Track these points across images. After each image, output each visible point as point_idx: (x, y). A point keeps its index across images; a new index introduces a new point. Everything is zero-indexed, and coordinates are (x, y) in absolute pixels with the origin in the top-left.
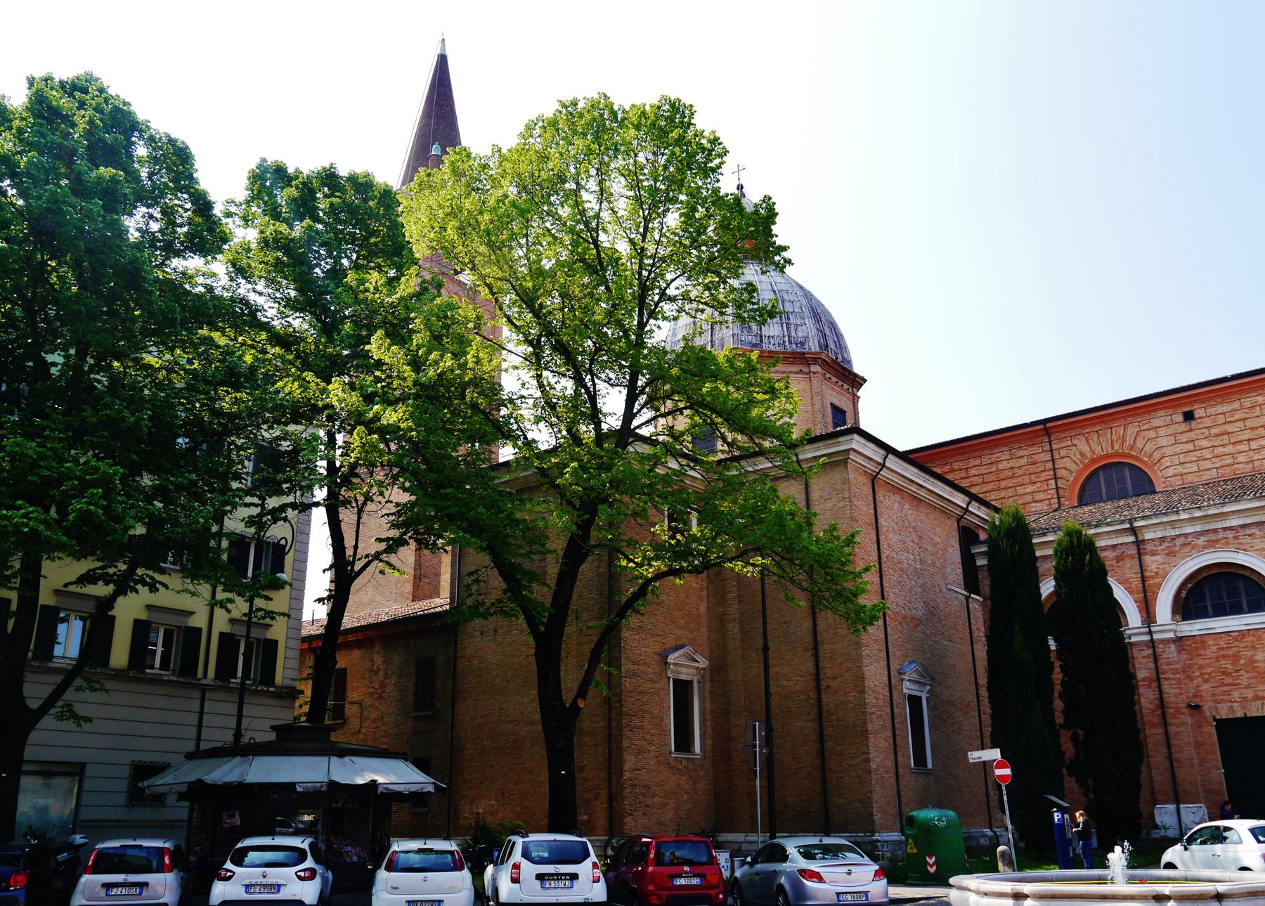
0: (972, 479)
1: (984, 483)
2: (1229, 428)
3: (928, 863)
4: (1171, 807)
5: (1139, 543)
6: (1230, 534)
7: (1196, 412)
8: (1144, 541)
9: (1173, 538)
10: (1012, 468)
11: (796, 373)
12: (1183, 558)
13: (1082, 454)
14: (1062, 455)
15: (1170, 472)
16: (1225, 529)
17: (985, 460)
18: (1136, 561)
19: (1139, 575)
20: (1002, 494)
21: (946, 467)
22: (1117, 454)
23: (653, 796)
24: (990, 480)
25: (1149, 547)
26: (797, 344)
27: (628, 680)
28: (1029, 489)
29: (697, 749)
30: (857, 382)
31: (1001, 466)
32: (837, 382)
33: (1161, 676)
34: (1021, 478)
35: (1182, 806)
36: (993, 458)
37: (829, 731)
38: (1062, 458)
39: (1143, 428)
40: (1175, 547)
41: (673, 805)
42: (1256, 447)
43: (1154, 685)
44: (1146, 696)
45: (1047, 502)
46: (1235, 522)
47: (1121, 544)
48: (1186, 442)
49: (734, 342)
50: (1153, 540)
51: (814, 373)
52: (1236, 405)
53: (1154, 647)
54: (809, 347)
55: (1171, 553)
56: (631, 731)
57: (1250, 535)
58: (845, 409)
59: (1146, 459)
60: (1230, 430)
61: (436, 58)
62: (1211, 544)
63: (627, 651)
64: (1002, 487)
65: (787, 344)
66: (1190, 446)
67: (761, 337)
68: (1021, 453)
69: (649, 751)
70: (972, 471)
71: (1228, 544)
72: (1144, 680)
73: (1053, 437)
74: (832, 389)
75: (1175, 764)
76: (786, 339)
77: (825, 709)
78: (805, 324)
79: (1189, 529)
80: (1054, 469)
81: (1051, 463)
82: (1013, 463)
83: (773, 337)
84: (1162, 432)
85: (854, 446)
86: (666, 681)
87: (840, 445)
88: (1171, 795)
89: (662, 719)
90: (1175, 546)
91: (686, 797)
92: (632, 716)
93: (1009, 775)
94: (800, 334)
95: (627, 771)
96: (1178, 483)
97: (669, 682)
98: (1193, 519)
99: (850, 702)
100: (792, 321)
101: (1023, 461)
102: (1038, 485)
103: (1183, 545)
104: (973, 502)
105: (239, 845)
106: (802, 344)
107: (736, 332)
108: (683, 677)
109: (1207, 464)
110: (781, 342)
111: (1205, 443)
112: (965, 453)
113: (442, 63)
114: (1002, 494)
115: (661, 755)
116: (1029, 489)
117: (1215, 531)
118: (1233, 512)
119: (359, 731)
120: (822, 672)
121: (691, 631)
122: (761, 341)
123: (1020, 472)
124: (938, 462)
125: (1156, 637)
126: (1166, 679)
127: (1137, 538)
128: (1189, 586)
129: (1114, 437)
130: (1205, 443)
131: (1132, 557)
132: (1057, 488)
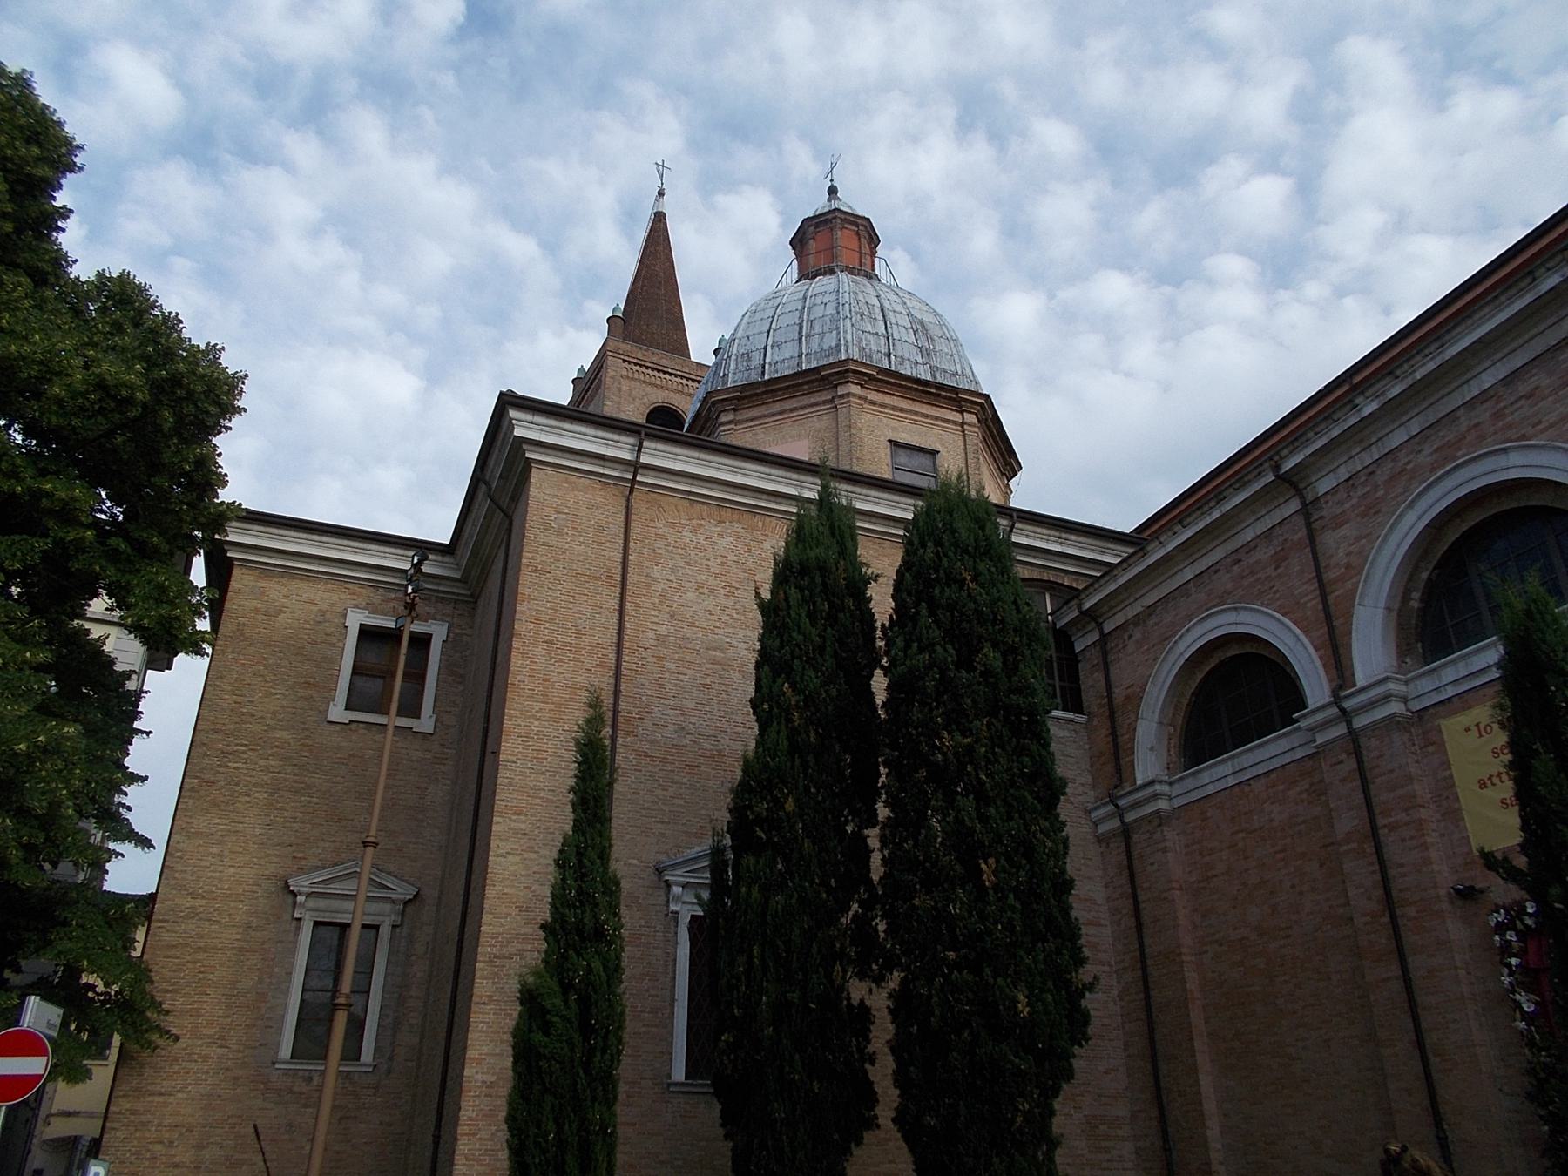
5: (1306, 511)
6: (1483, 413)
16: (1470, 404)
25: (1329, 510)
33: (1381, 821)
43: (1370, 848)
53: (1357, 752)
57: (1528, 397)
71: (1482, 438)
75: (1433, 1060)
78: (838, 328)
90: (1376, 488)
117: (1451, 416)
125: (1360, 722)
126: (1392, 828)
127: (1303, 498)
128: (1425, 575)
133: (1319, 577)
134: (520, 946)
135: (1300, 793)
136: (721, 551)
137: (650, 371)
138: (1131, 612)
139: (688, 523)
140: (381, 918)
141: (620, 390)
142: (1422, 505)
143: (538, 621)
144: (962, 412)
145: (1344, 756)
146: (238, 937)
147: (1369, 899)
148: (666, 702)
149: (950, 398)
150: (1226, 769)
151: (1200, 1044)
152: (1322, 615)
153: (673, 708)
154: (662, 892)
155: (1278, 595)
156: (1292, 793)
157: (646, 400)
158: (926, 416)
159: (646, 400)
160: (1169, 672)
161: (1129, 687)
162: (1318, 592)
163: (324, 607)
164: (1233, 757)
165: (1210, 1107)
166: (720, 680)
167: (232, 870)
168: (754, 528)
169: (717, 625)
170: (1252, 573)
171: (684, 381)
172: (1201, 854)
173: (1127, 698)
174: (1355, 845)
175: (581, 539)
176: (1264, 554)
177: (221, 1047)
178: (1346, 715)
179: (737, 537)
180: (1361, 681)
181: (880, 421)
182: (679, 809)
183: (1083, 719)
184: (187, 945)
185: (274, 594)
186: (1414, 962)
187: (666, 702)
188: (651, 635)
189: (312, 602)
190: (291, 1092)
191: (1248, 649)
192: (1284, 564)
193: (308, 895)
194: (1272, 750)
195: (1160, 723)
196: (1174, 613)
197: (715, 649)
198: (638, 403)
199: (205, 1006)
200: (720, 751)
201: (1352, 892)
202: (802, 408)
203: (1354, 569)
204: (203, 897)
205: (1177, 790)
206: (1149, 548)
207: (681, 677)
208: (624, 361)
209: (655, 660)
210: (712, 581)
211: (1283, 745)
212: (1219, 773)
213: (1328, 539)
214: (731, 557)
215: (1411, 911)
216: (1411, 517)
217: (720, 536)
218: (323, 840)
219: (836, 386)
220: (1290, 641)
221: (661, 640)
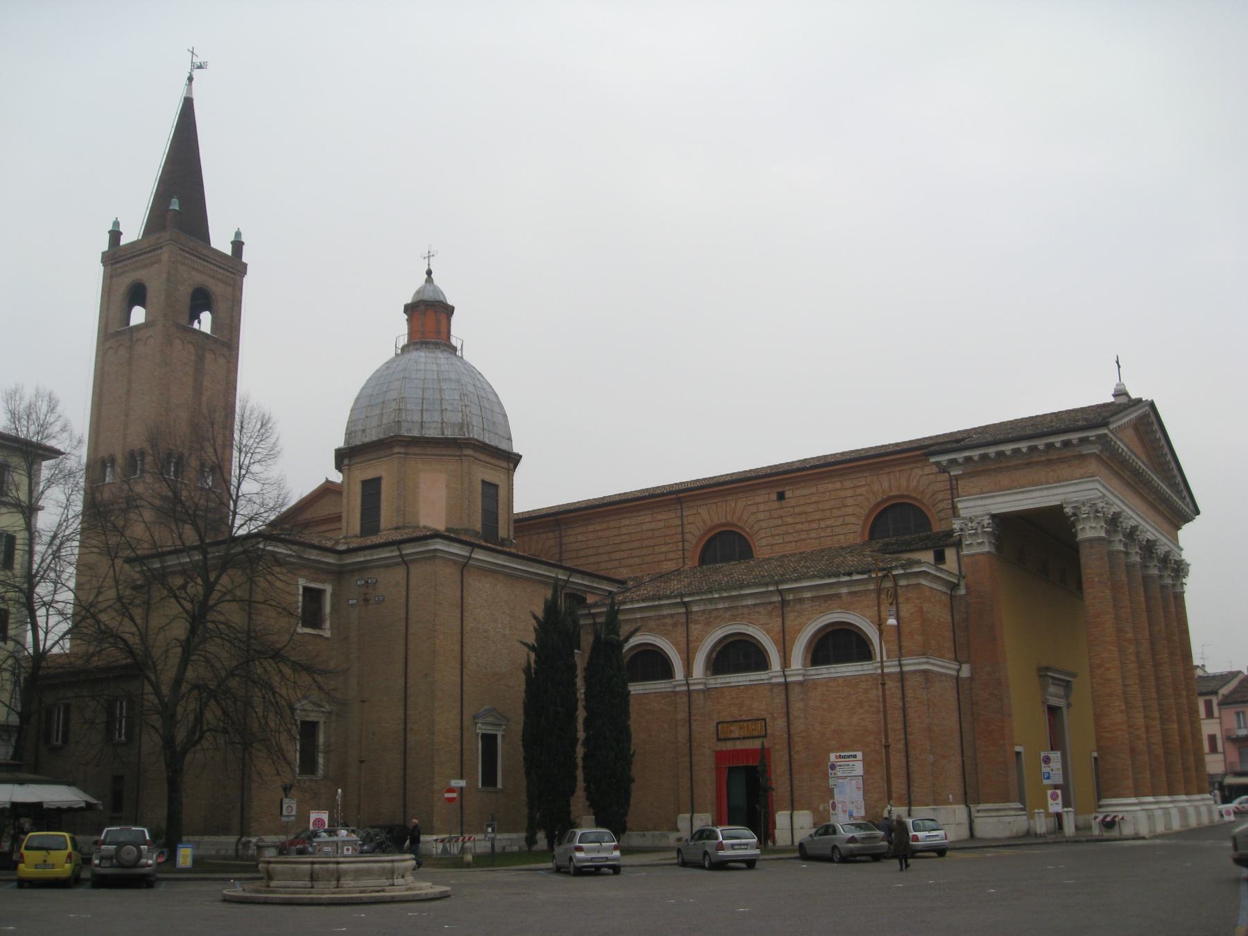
2: (808, 509)
4: (688, 816)
5: (688, 613)
6: (746, 611)
7: (786, 493)
9: (710, 612)
10: (653, 530)
12: (715, 628)
13: (704, 522)
14: (690, 521)
15: (764, 542)
16: (743, 606)
18: (685, 628)
19: (686, 639)
22: (727, 524)
28: (664, 549)
30: (514, 459)
31: (645, 527)
33: (692, 718)
35: (913, 808)
38: (690, 524)
39: (749, 503)
40: (711, 621)
42: (824, 526)
43: (688, 725)
45: (675, 561)
46: (750, 602)
47: (677, 614)
48: (778, 518)
50: (697, 612)
51: (465, 456)
52: (814, 490)
55: (708, 624)
59: (748, 530)
60: (808, 510)
61: (183, 99)
62: (734, 618)
66: (779, 522)
68: (660, 517)
70: (624, 530)
71: (743, 618)
73: (684, 506)
75: (694, 784)
79: (721, 606)
80: (683, 533)
81: (680, 528)
84: (762, 507)
85: (438, 547)
88: (907, 802)
96: (768, 552)
98: (722, 599)
101: (661, 524)
102: (670, 546)
103: (716, 618)
109: (789, 538)
111: (790, 520)
116: (664, 549)
117: (737, 607)
118: (748, 594)
125: (692, 688)
126: (695, 720)
127: (687, 610)
128: (718, 649)
129: (728, 508)
130: (790, 520)
132: (684, 550)
133: (687, 637)
142: (724, 630)
144: (508, 462)
145: (684, 696)
150: (641, 687)
170: (664, 626)
176: (669, 621)
178: (688, 684)
180: (694, 677)
183: (581, 652)
186: (694, 758)
202: (444, 455)
203: (700, 640)
208: (180, 249)
213: (692, 627)
215: (696, 744)
216: (719, 632)
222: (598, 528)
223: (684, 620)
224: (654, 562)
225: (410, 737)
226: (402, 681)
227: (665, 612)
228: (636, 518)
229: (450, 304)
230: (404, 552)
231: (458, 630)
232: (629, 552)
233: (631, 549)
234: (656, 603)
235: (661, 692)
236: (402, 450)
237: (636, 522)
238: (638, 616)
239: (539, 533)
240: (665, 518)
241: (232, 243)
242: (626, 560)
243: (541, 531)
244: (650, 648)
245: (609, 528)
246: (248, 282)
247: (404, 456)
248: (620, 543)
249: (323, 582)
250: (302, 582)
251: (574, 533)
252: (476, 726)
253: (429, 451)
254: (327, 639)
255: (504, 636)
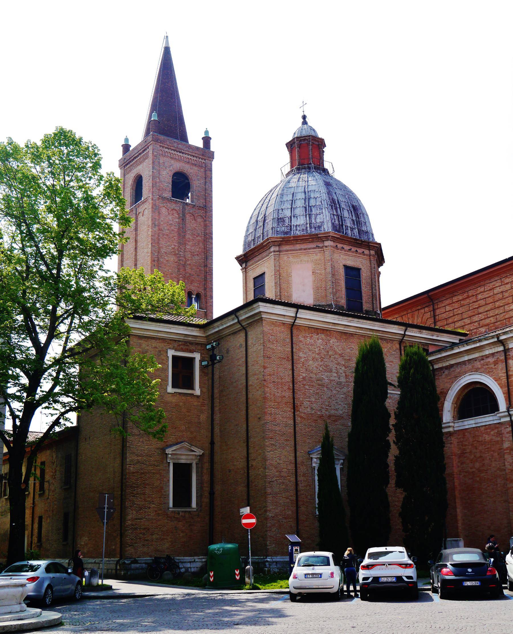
0: (479, 302)
1: (486, 304)
3: (236, 574)
8: (509, 349)
10: (502, 292)
11: (313, 248)
17: (487, 288)
20: (497, 312)
21: (465, 295)
23: (152, 535)
24: (489, 302)
26: (315, 228)
27: (132, 466)
29: (194, 504)
31: (496, 291)
32: (350, 250)
34: (507, 299)
36: (491, 285)
37: (252, 493)
41: (170, 540)
44: (508, 460)
47: (497, 352)
49: (272, 233)
51: (326, 247)
54: (324, 228)
56: (134, 496)
58: (360, 266)
61: (163, 49)
63: (131, 449)
64: (496, 306)
65: (308, 229)
67: (291, 226)
69: (149, 508)
70: (480, 297)
72: (507, 449)
74: (346, 255)
76: (308, 225)
77: (250, 479)
78: (322, 213)
82: (503, 288)
83: (299, 226)
85: (261, 309)
86: (167, 465)
87: (255, 310)
89: (162, 488)
91: (182, 534)
92: (135, 487)
93: (243, 519)
94: (318, 220)
95: (129, 520)
97: (169, 465)
99: (260, 475)
100: (314, 212)
104: (408, 329)
105: (257, 585)
106: (319, 227)
107: (274, 226)
108: (183, 460)
110: (305, 228)
112: (476, 283)
113: (167, 52)
114: (497, 312)
115: (161, 510)
119: (48, 498)
120: (250, 455)
121: (192, 433)
122: (291, 229)
123: (506, 294)
124: (460, 292)
127: (504, 347)
131: (501, 361)
133: (507, 372)
134: (276, 478)
135: (494, 433)
136: (318, 345)
137: (173, 152)
138: (444, 365)
139: (308, 335)
140: (192, 461)
141: (159, 163)
143: (270, 375)
144: (369, 250)
145: (508, 426)
146: (152, 469)
147: (511, 466)
148: (307, 399)
149: (366, 245)
150: (472, 422)
151: (458, 501)
152: (506, 384)
153: (309, 401)
154: (310, 460)
155: (494, 374)
156: (492, 433)
157: (171, 168)
158: (140, 154)
159: (171, 168)
160: (457, 388)
161: (442, 389)
162: (506, 377)
163: (160, 349)
164: (475, 419)
165: (459, 518)
166: (321, 391)
167: (147, 447)
168: (327, 335)
169: (319, 371)
170: (487, 365)
171: (189, 157)
172: (462, 445)
173: (441, 392)
174: (508, 451)
175: (279, 345)
176: (491, 360)
177: (153, 504)
179: (322, 339)
181: (340, 256)
182: (313, 434)
184: (138, 472)
185: (144, 346)
187: (307, 399)
188: (301, 377)
189: (156, 348)
190: (174, 517)
191: (482, 386)
192: (497, 365)
193: (171, 454)
194: (487, 419)
195: (452, 403)
196: (460, 369)
197: (319, 380)
198: (168, 169)
199: (146, 491)
200: (322, 415)
201: (506, 463)
202: (309, 249)
204: (140, 456)
205: (456, 425)
206: (455, 348)
207: (311, 391)
209: (302, 386)
210: (317, 356)
211: (491, 418)
212: (470, 423)
214: (322, 347)
217: (318, 339)
218: (172, 435)
219: (323, 241)
220: (497, 389)
221: (304, 378)
222: (460, 298)
223: (503, 358)
224: (505, 319)
225: (251, 472)
226: (245, 426)
227: (487, 352)
228: (488, 285)
229: (320, 136)
230: (241, 318)
231: (289, 379)
232: (485, 313)
233: (487, 311)
234: (478, 345)
235: (490, 424)
236: (277, 249)
237: (489, 288)
238: (466, 358)
239: (418, 310)
240: (511, 281)
241: (203, 138)
242: (483, 321)
243: (419, 307)
244: (478, 386)
245: (468, 297)
246: (216, 165)
247: (278, 253)
248: (478, 308)
249: (192, 351)
250: (171, 353)
251: (443, 305)
252: (312, 461)
253: (298, 246)
254: (198, 397)
255: (339, 383)
